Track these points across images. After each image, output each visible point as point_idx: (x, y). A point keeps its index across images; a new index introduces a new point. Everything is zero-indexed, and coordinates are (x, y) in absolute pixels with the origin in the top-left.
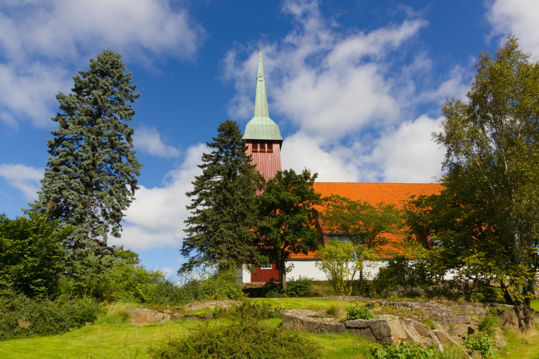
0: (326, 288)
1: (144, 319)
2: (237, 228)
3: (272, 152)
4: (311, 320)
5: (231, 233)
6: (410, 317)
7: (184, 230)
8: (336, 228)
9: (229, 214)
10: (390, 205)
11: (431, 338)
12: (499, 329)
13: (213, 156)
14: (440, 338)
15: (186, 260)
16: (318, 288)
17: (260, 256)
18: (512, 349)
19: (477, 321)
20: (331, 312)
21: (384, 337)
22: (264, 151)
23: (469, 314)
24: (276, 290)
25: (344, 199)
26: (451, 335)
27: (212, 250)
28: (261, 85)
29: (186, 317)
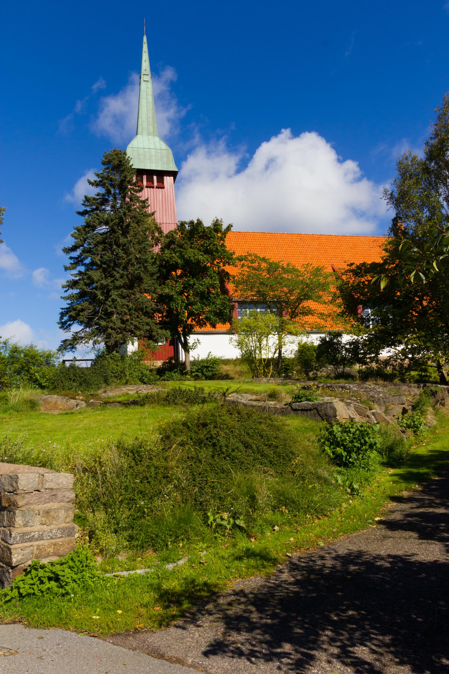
0: (238, 368)
1: (55, 406)
2: (133, 296)
3: (163, 188)
4: (254, 403)
5: (125, 301)
6: (350, 399)
7: (61, 297)
8: (251, 295)
9: (122, 277)
10: (318, 267)
11: (369, 418)
12: (431, 409)
13: (98, 199)
14: (377, 418)
15: (68, 335)
16: (228, 369)
17: (160, 331)
18: (442, 427)
19: (411, 402)
20: (273, 396)
21: (330, 417)
22: (152, 185)
23: (404, 394)
24: (177, 372)
25: (264, 259)
26: (386, 416)
27: (103, 323)
28: (147, 88)
29: (106, 403)
